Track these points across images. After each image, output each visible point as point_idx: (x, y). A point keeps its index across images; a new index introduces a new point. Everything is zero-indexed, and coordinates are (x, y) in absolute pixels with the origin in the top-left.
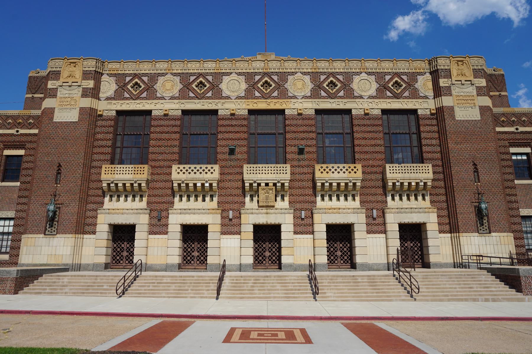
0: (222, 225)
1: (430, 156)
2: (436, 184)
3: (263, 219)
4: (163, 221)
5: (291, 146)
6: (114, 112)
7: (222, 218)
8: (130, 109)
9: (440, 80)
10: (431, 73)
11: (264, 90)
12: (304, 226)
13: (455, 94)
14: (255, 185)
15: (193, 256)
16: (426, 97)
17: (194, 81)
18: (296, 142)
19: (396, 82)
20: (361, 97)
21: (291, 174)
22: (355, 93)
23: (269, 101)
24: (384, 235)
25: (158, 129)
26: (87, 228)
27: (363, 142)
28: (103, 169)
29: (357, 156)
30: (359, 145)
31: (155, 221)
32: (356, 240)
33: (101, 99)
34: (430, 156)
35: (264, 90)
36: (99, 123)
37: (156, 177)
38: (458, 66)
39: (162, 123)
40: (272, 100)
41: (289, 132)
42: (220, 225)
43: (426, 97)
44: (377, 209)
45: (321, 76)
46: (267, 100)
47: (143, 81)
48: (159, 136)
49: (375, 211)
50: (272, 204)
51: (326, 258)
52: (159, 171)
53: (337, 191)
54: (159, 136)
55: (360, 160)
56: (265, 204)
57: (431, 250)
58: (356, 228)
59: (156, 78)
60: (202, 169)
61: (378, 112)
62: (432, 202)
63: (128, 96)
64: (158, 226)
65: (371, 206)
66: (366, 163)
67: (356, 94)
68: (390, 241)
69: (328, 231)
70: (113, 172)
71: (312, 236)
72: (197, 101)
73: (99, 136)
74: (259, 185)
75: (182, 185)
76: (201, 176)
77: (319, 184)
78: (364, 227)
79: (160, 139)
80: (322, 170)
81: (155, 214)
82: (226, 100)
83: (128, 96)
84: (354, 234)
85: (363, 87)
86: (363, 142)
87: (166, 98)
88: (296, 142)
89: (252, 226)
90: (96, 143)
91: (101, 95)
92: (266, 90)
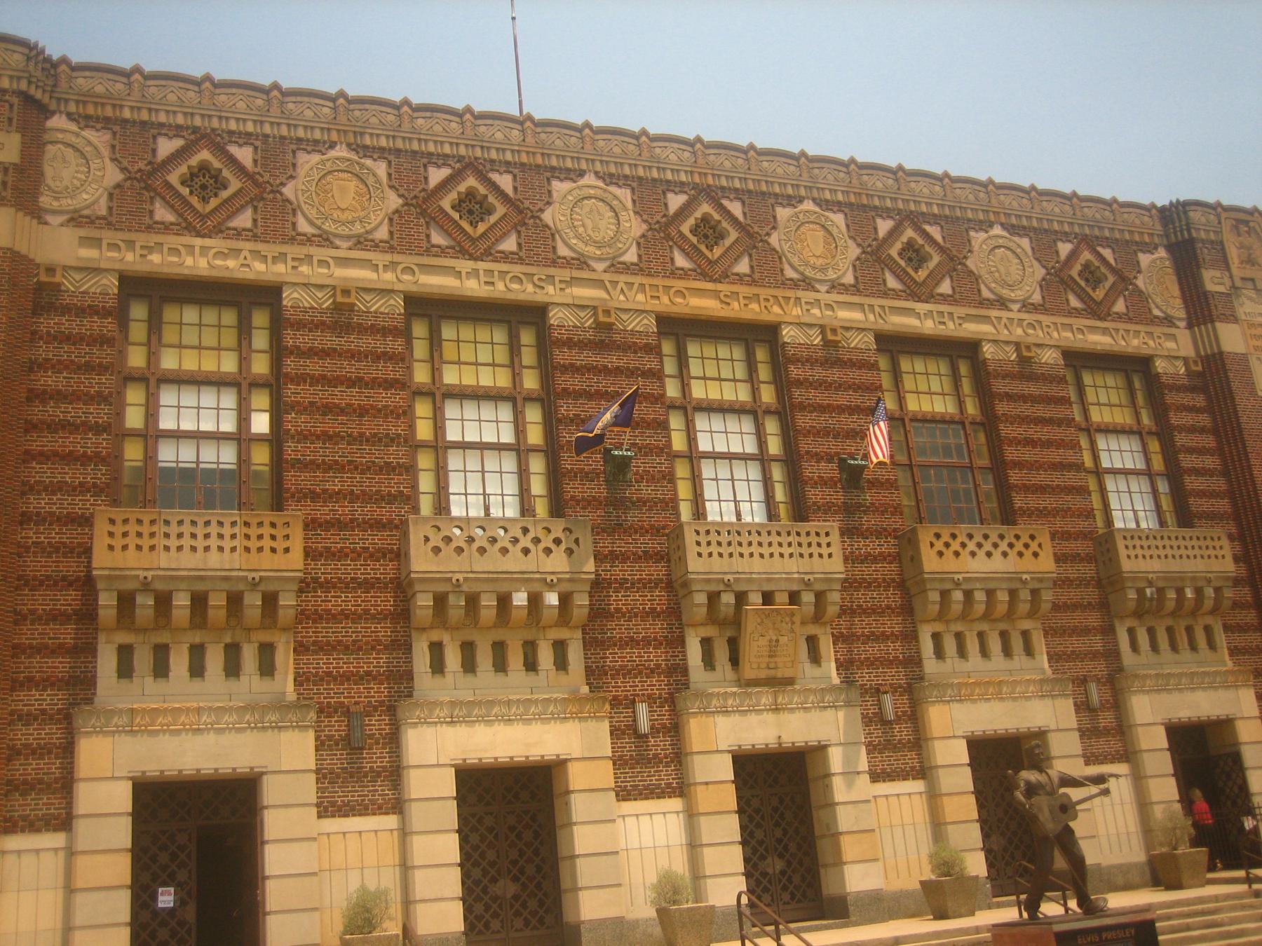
0: (619, 762)
1: (1033, 501)
2: (863, 598)
3: (763, 729)
4: (376, 758)
5: (818, 457)
6: (871, 338)
7: (615, 732)
8: (247, 275)
9: (1203, 270)
10: (1170, 248)
11: (194, 201)
12: (1108, 733)
13: (1244, 317)
14: (728, 599)
15: (495, 899)
16: (1168, 321)
17: (444, 185)
18: (831, 445)
19: (705, 219)
20: (1002, 303)
21: (846, 559)
22: (559, 244)
23: (724, 288)
24: (917, 786)
25: (314, 367)
26: (21, 806)
27: (1028, 455)
28: (101, 528)
29: (1019, 501)
30: (1019, 465)
31: (338, 760)
32: (267, 847)
33: (49, 218)
34: (1033, 501)
35: (194, 201)
36: (48, 324)
37: (323, 570)
38: (1239, 235)
39: (330, 341)
40: (735, 288)
41: (802, 407)
42: (1077, 734)
43: (1168, 321)
44: (650, 700)
45: (670, 196)
46: (720, 287)
47: (233, 161)
48: (320, 394)
49: (642, 710)
50: (788, 673)
51: (457, 909)
52: (333, 540)
53: (495, 626)
54: (320, 394)
55: (1028, 513)
56: (763, 674)
57: (585, 871)
58: (271, 792)
59: (289, 157)
60: (531, 535)
61: (862, 342)
62: (1233, 652)
63: (170, 217)
64: (361, 773)
65: (622, 687)
66: (1059, 524)
67: (563, 251)
68: (417, 842)
69: (974, 764)
70: (146, 542)
71: (391, 821)
72: (465, 265)
73: (50, 380)
74: (741, 598)
75: (452, 599)
76: (529, 564)
77: (424, 601)
78: (308, 789)
79: (327, 409)
80: (939, 545)
81: (336, 727)
82: (576, 274)
83: (170, 217)
84: (567, 804)
85: (1002, 270)
86: (1028, 455)
87: (338, 242)
88: (831, 445)
89: (964, 741)
90: (38, 412)
91: (45, 200)
92: (205, 200)
